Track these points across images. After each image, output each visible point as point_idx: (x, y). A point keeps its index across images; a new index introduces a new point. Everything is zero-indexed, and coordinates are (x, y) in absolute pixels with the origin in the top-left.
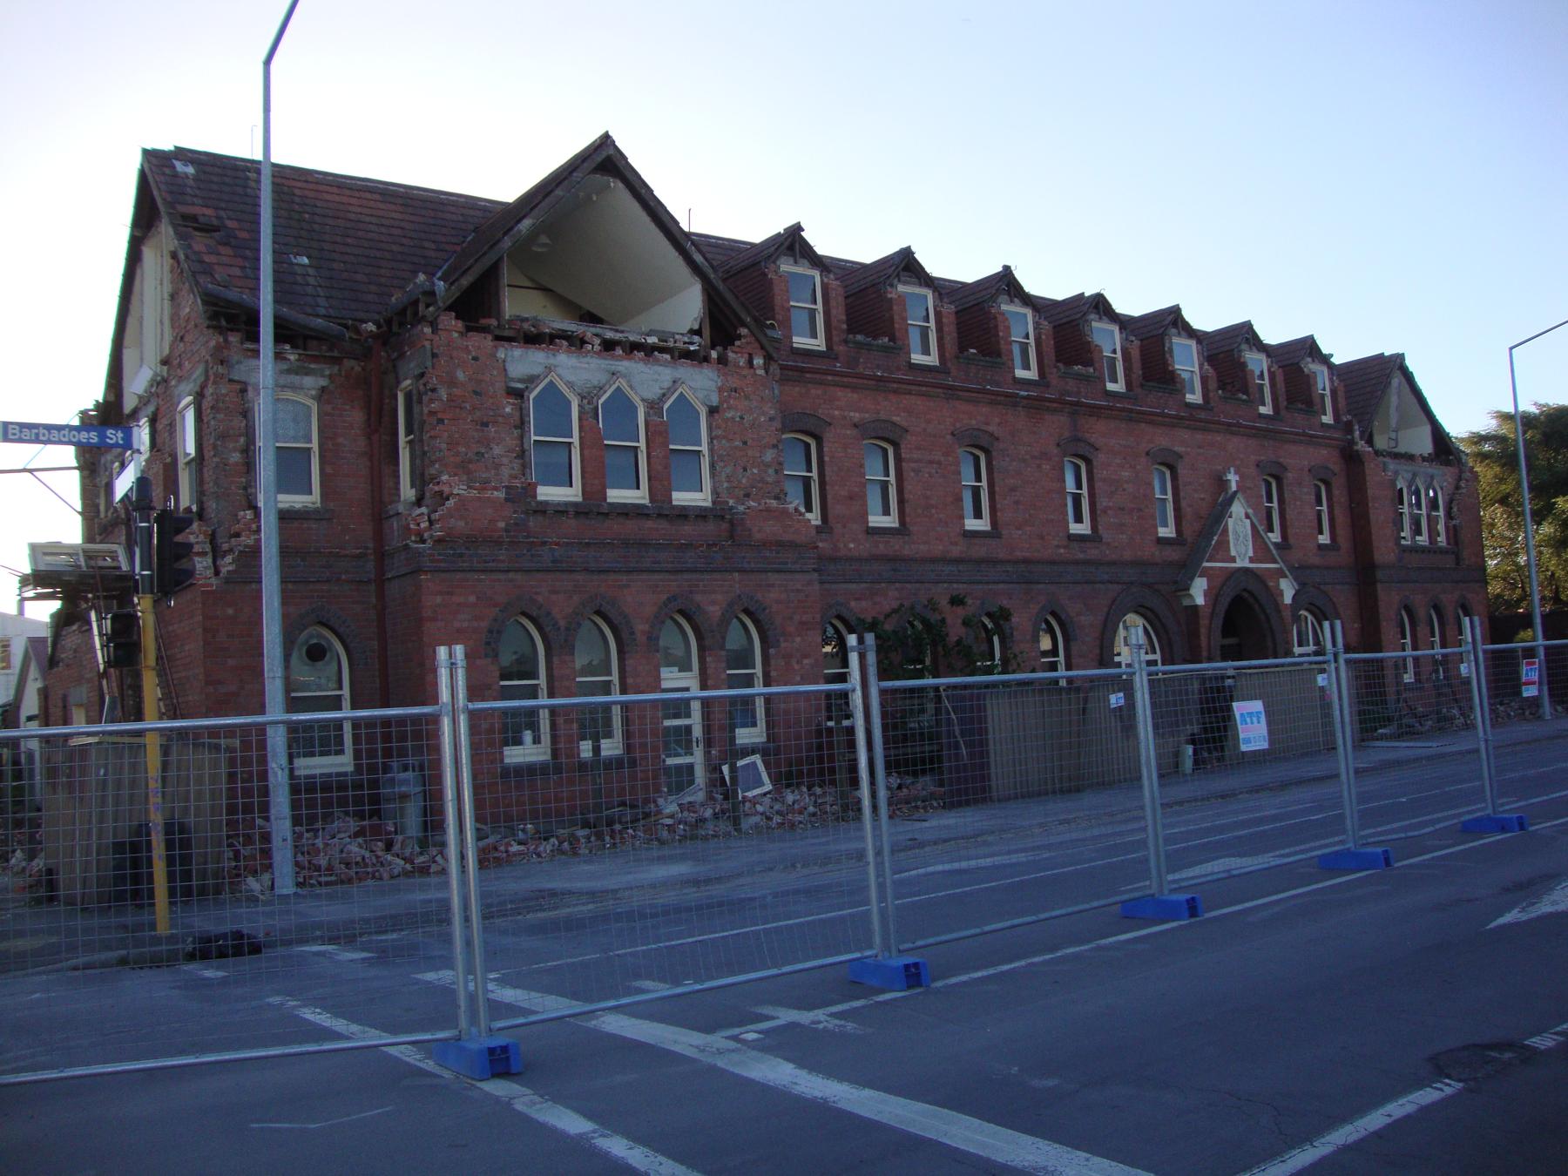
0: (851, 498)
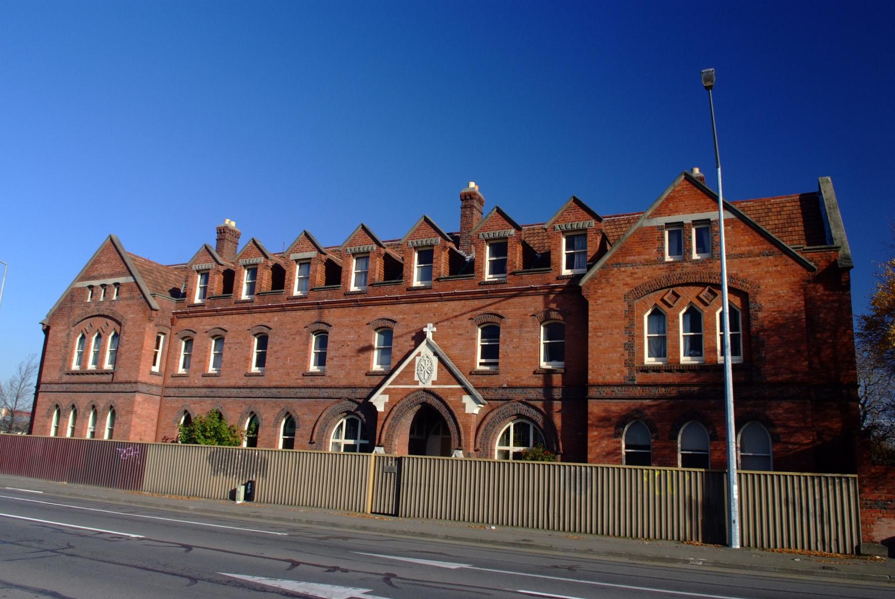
0: (200, 362)
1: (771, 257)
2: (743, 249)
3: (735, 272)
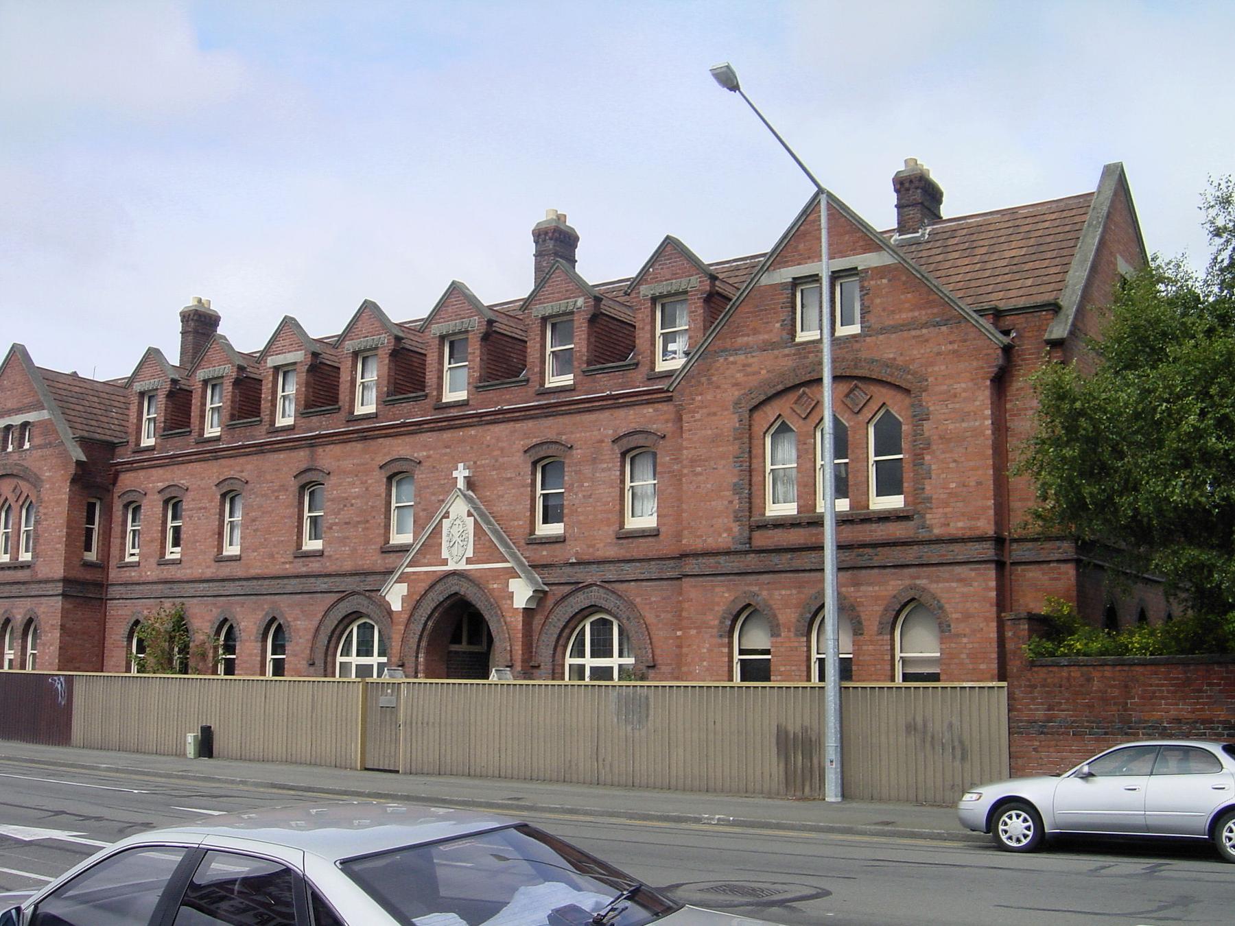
1: (944, 328)
2: (904, 316)
3: (891, 356)
